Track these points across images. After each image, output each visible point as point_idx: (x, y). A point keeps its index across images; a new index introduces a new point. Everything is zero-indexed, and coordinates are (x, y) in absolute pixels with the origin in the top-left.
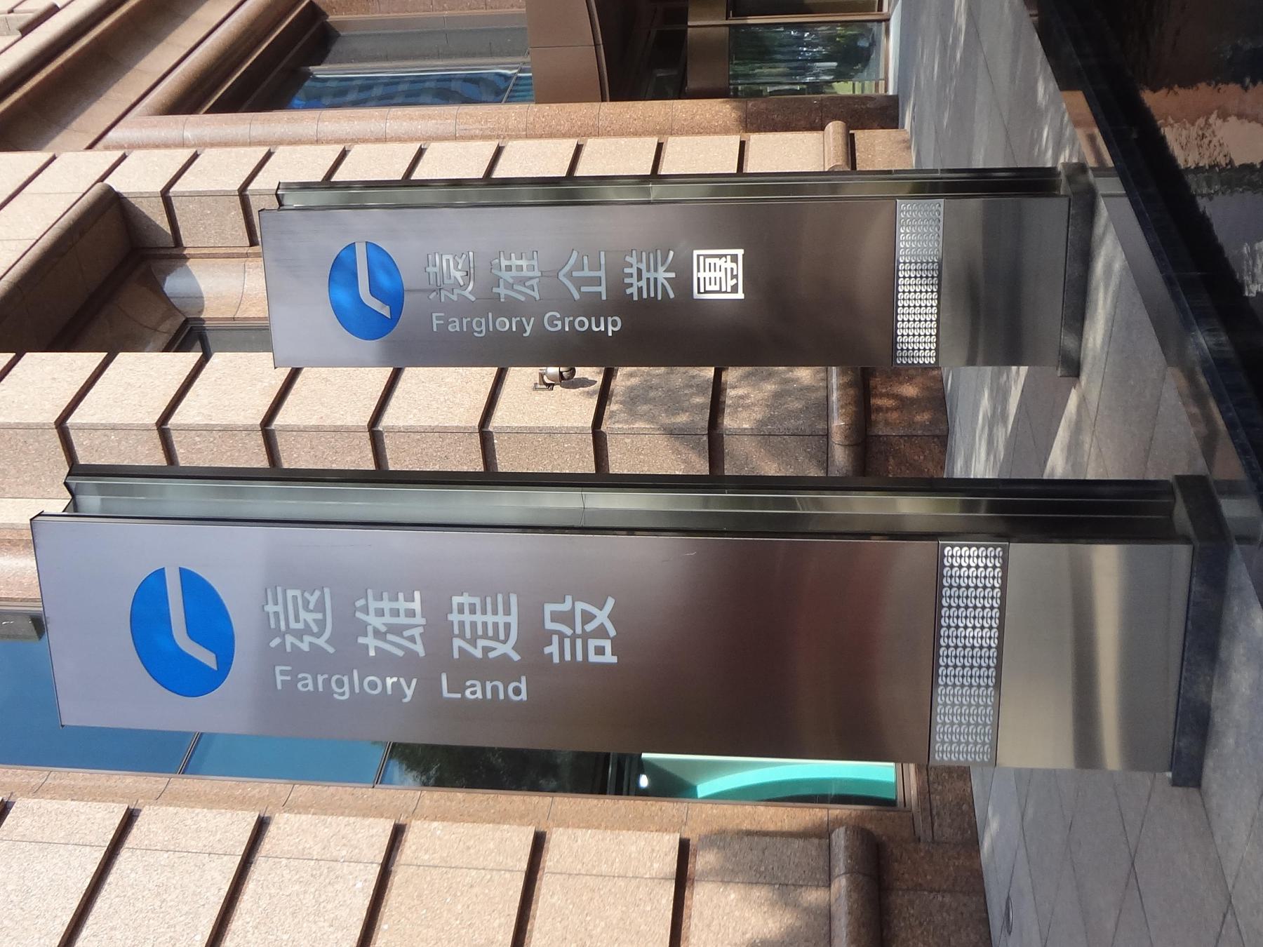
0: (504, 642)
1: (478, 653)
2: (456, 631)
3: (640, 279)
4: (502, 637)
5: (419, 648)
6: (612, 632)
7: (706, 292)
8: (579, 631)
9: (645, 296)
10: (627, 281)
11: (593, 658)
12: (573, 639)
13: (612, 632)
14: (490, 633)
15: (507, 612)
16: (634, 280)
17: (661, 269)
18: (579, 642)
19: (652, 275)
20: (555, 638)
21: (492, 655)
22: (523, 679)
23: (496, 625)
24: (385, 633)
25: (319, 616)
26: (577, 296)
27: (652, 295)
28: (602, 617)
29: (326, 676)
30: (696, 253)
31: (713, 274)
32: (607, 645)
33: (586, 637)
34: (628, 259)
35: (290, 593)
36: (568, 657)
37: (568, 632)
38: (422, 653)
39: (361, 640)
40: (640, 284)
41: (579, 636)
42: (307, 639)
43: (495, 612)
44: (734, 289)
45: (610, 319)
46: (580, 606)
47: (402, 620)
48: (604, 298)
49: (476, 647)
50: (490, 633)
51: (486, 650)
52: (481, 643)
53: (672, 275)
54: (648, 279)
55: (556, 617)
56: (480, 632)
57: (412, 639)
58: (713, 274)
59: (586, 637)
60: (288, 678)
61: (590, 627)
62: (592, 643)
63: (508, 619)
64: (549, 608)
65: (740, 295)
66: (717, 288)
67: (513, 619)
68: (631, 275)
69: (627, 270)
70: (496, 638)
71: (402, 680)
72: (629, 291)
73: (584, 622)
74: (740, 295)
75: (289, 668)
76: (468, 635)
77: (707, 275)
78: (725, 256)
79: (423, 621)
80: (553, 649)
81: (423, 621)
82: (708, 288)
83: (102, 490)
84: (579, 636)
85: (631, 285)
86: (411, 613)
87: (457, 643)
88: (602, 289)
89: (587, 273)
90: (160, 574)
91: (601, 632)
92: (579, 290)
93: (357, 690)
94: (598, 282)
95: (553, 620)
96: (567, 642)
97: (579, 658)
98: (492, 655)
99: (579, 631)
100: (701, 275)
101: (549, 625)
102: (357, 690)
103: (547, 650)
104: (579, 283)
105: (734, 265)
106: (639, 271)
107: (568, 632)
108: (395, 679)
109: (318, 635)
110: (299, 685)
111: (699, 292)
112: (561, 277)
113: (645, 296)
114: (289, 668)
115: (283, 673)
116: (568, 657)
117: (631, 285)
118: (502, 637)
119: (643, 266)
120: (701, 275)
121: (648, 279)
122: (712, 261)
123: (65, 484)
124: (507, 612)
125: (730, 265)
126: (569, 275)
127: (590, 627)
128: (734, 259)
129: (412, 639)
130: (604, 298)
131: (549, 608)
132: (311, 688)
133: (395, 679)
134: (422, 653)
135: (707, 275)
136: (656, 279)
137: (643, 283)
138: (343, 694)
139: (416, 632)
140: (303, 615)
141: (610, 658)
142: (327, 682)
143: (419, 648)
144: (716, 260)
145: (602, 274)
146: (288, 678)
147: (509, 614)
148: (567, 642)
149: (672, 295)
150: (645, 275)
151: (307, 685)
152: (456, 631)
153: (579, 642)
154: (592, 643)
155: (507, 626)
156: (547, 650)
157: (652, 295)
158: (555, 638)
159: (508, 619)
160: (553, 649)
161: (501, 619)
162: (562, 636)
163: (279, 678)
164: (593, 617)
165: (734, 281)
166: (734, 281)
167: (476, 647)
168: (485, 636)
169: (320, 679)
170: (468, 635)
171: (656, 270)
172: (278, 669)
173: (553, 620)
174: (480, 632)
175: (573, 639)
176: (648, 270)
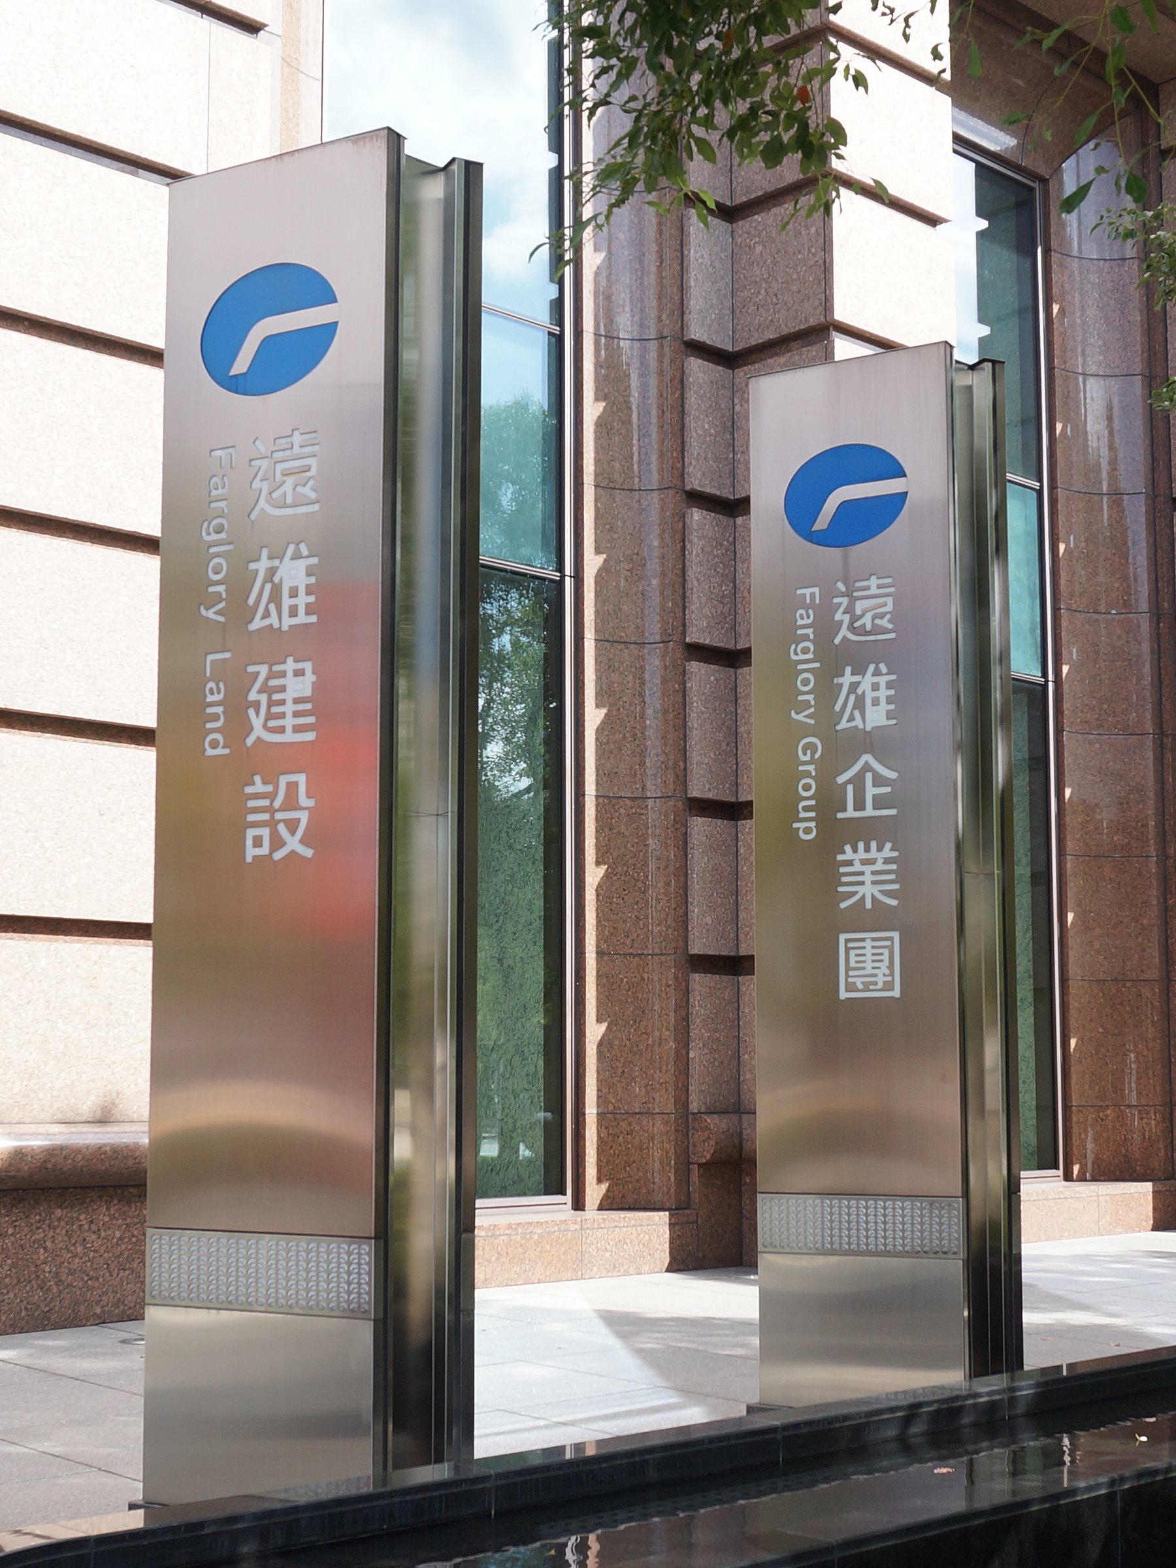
0: (265, 727)
1: (253, 696)
2: (276, 668)
3: (864, 862)
4: (271, 724)
5: (843, 725)
6: (278, 855)
7: (847, 950)
8: (279, 816)
9: (842, 870)
10: (861, 845)
11: (251, 833)
12: (270, 810)
13: (278, 855)
14: (274, 710)
15: (297, 729)
16: (862, 855)
17: (875, 890)
18: (265, 817)
19: (868, 878)
20: (270, 788)
21: (251, 712)
22: (227, 751)
23: (282, 716)
24: (272, 581)
25: (289, 500)
26: (841, 779)
27: (844, 879)
28: (293, 843)
29: (812, 637)
30: (896, 935)
31: (869, 958)
32: (264, 850)
33: (272, 824)
34: (888, 845)
35: (312, 462)
36: (251, 804)
37: (277, 804)
38: (839, 727)
39: (848, 670)
40: (857, 863)
41: (272, 816)
42: (847, 618)
43: (296, 714)
44: (851, 988)
45: (813, 824)
46: (304, 816)
47: (287, 602)
48: (840, 815)
49: (259, 692)
50: (274, 710)
51: (256, 705)
52: (264, 698)
53: (869, 905)
54: (862, 873)
55: (292, 787)
56: (276, 697)
57: (851, 719)
58: (869, 958)
59: (272, 824)
60: (808, 601)
61: (281, 828)
62: (265, 832)
63: (289, 729)
64: (301, 779)
65: (843, 995)
66: (853, 964)
67: (289, 737)
68: (867, 850)
69: (874, 844)
70: (270, 716)
71: (812, 710)
72: (848, 848)
73: (287, 822)
74: (843, 995)
75: (817, 601)
76: (272, 683)
77: (869, 951)
78: (892, 974)
79: (285, 628)
80: (259, 786)
81: (285, 628)
82: (852, 953)
83: (448, 202)
84: (272, 816)
85: (855, 851)
86: (293, 612)
87: (263, 670)
88: (850, 813)
89: (870, 791)
90: (326, 295)
91: (277, 842)
92: (849, 782)
93: (800, 667)
94: (860, 805)
95: (289, 784)
96: (265, 803)
97: (251, 818)
98: (251, 712)
99: (279, 816)
100: (868, 944)
101: (284, 780)
102: (800, 667)
103: (257, 779)
104: (858, 782)
105: (880, 986)
106: (873, 862)
107: (277, 804)
108: (813, 703)
109: (852, 629)
110: (801, 611)
111: (847, 941)
112: (867, 758)
113: (842, 870)
114: (817, 601)
115: (813, 595)
116: (251, 804)
117: (855, 851)
118: (271, 724)
119: (879, 866)
120: (868, 944)
121: (862, 873)
122: (886, 957)
123: (453, 160)
124: (297, 729)
125: (881, 980)
126: (867, 768)
127: (281, 828)
128: (889, 986)
129: (851, 719)
130: (840, 815)
131: (301, 779)
132: (800, 622)
133: (813, 703)
134: (839, 727)
135: (869, 951)
136: (862, 883)
137: (857, 867)
138: (797, 654)
139: (273, 620)
140: (290, 481)
141: (251, 852)
142: (806, 638)
143: (843, 725)
144: (886, 962)
145: (869, 811)
146: (808, 601)
147: (284, 727)
148: (265, 803)
149: (843, 905)
150: (868, 869)
151: (802, 618)
152: (276, 668)
153: (265, 817)
154: (265, 832)
155: (281, 730)
156: (257, 779)
157: (844, 879)
158: (270, 788)
159: (289, 729)
160: (259, 786)
161: (289, 722)
162: (272, 796)
163: (807, 591)
164: (293, 830)
165: (860, 986)
166: (860, 986)
167: (259, 692)
168: (271, 704)
169: (809, 631)
170: (272, 683)
171: (874, 883)
172: (816, 590)
173: (289, 784)
174: (276, 697)
175: (270, 810)
176: (873, 873)
